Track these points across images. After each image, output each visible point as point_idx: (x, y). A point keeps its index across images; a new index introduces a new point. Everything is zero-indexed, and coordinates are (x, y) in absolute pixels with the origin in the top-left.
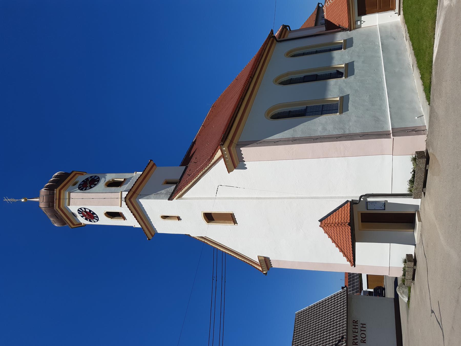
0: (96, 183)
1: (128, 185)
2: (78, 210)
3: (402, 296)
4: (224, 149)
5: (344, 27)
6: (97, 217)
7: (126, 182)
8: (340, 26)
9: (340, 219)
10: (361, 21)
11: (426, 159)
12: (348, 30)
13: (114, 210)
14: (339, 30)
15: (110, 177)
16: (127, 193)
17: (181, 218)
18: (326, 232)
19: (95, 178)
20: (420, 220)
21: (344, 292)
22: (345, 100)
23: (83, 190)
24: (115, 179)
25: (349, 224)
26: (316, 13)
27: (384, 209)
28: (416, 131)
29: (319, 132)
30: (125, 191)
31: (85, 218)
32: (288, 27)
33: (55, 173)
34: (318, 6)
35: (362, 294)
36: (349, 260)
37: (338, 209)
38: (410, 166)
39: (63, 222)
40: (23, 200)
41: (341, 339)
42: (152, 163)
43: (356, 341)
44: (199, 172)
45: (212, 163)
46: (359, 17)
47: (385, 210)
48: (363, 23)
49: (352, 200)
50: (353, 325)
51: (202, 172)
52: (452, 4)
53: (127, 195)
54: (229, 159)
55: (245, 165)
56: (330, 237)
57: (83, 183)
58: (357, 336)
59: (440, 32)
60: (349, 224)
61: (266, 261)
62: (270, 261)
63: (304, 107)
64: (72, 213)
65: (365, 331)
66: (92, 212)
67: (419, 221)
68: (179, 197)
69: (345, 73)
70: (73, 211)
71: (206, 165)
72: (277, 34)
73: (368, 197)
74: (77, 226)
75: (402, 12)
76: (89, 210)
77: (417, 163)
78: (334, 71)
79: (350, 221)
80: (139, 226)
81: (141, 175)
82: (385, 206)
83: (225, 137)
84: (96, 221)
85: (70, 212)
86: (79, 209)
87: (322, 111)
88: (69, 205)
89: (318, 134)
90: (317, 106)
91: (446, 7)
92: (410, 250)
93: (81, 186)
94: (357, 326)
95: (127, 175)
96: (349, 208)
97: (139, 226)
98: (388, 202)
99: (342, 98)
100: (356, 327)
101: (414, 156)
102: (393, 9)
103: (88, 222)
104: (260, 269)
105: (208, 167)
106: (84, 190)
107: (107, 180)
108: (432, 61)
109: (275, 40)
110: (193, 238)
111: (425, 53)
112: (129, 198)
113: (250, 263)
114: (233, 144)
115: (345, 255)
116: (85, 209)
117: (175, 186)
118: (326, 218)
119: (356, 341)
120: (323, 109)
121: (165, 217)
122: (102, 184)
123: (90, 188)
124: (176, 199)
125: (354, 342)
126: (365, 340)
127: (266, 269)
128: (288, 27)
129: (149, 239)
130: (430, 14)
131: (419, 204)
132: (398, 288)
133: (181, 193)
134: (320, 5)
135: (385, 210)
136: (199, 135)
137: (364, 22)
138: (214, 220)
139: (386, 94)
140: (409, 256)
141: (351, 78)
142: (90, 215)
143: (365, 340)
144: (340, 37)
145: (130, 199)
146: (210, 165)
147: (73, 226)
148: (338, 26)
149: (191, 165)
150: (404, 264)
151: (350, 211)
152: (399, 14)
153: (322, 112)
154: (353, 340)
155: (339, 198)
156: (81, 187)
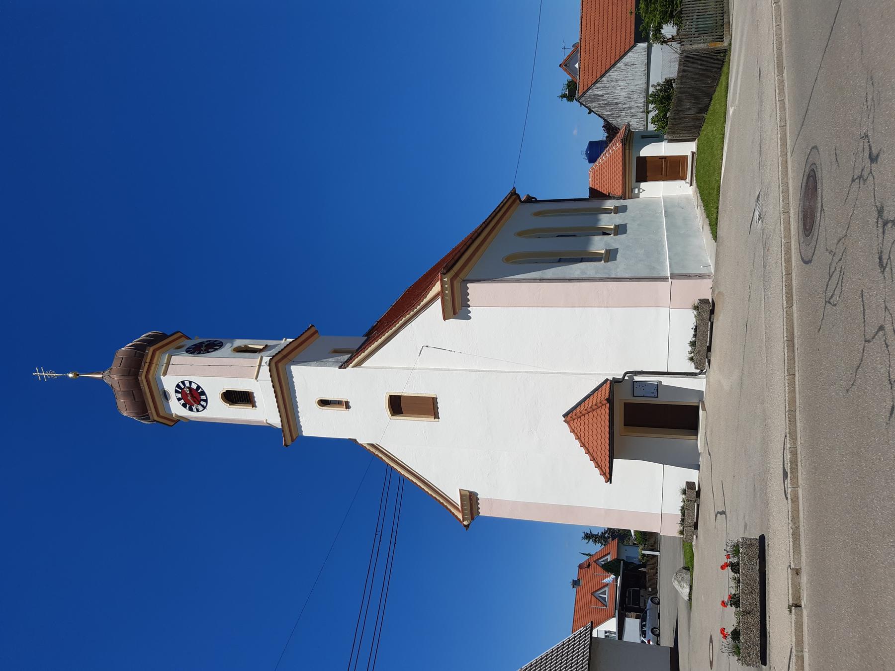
4: (446, 280)
6: (206, 401)
8: (610, 195)
10: (639, 189)
15: (239, 343)
19: (216, 343)
24: (250, 346)
27: (656, 396)
29: (577, 274)
31: (183, 402)
36: (603, 473)
39: (142, 410)
40: (71, 375)
46: (638, 183)
48: (641, 192)
49: (613, 378)
51: (404, 319)
54: (449, 304)
55: (470, 312)
61: (471, 500)
62: (477, 502)
64: (165, 391)
70: (166, 388)
74: (161, 421)
75: (694, 182)
84: (200, 408)
88: (165, 374)
89: (576, 276)
92: (693, 476)
98: (663, 384)
102: (683, 178)
103: (184, 412)
104: (460, 516)
109: (518, 200)
110: (361, 447)
112: (275, 361)
113: (445, 504)
115: (598, 466)
116: (190, 383)
118: (573, 411)
121: (324, 403)
122: (227, 348)
124: (353, 367)
127: (469, 517)
129: (286, 445)
131: (704, 389)
135: (657, 397)
137: (644, 190)
138: (403, 413)
139: (666, 250)
140: (690, 485)
144: (610, 204)
145: (277, 364)
147: (156, 418)
148: (608, 194)
152: (691, 185)
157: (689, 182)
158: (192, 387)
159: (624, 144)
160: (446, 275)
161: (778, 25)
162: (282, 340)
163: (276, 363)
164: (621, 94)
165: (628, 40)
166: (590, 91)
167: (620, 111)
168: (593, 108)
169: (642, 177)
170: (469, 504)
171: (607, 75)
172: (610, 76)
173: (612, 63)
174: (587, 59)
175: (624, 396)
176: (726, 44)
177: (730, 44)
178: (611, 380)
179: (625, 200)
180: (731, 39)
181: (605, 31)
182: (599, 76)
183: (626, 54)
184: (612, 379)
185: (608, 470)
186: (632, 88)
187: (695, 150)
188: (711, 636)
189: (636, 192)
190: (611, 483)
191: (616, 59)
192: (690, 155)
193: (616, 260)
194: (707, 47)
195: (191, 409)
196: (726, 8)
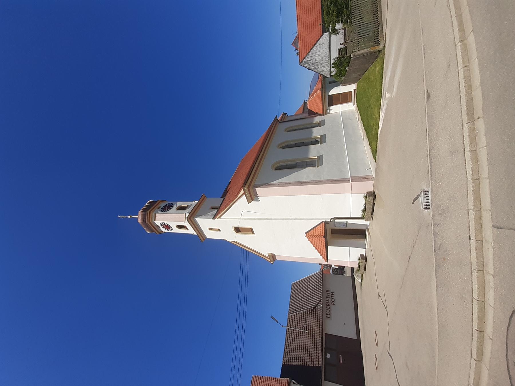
0: (171, 207)
1: (189, 209)
2: (161, 224)
3: (357, 278)
4: (245, 189)
5: (351, 9)
6: (172, 228)
7: (188, 207)
9: (318, 233)
10: (330, 110)
11: (373, 197)
12: (322, 115)
14: (317, 115)
15: (179, 204)
16: (188, 214)
17: (220, 230)
18: (309, 240)
20: (369, 234)
21: (321, 272)
22: (320, 158)
24: (183, 206)
25: (324, 237)
26: (303, 106)
28: (366, 178)
30: (187, 213)
32: (286, 114)
33: (148, 201)
34: (305, 102)
35: (331, 271)
37: (317, 226)
38: (363, 201)
40: (129, 217)
41: (319, 302)
42: (204, 196)
43: (328, 303)
44: (230, 202)
45: (238, 197)
46: (329, 107)
47: (346, 227)
50: (327, 293)
52: (392, 96)
53: (188, 216)
54: (248, 195)
55: (259, 199)
56: (312, 243)
58: (329, 300)
59: (384, 114)
60: (324, 237)
61: (273, 256)
63: (295, 162)
65: (334, 297)
67: (369, 235)
68: (219, 218)
69: (321, 141)
70: (157, 224)
71: (234, 199)
72: (279, 118)
73: (336, 219)
75: (356, 103)
77: (368, 199)
78: (314, 140)
80: (196, 234)
81: (197, 203)
82: (346, 225)
83: (246, 182)
84: (171, 230)
88: (155, 221)
89: (304, 180)
91: (388, 99)
94: (329, 293)
95: (189, 203)
96: (324, 226)
97: (196, 234)
99: (318, 157)
100: (329, 294)
101: (365, 194)
102: (350, 101)
103: (166, 231)
105: (236, 200)
107: (177, 206)
108: (378, 134)
111: (372, 129)
114: (251, 186)
115: (321, 255)
116: (164, 223)
117: (216, 210)
119: (328, 303)
121: (211, 229)
122: (175, 208)
124: (217, 219)
125: (327, 304)
126: (334, 303)
127: (273, 261)
128: (286, 114)
129: (202, 242)
130: (376, 104)
131: (369, 224)
132: (354, 273)
133: (220, 215)
134: (306, 101)
136: (233, 178)
137: (332, 110)
138: (240, 231)
141: (324, 145)
142: (168, 227)
143: (334, 303)
144: (317, 120)
145: (190, 218)
146: (237, 199)
147: (158, 233)
149: (227, 197)
150: (359, 261)
151: (325, 228)
153: (306, 166)
154: (327, 302)
155: (317, 219)
156: (162, 210)
157: (353, 103)
159: (322, 91)
160: (245, 187)
161: (466, 66)
162: (193, 201)
163: (189, 218)
164: (318, 58)
165: (319, 32)
166: (305, 59)
167: (318, 65)
168: (307, 66)
169: (331, 104)
170: (272, 259)
171: (311, 51)
172: (313, 51)
173: (313, 45)
174: (302, 44)
175: (332, 226)
176: (381, 47)
177: (384, 47)
178: (325, 222)
179: (324, 116)
180: (385, 43)
181: (309, 29)
182: (308, 52)
183: (319, 40)
185: (326, 257)
186: (323, 54)
187: (355, 87)
189: (329, 111)
191: (315, 43)
192: (353, 90)
193: (323, 165)
194: (369, 51)
196: (380, 21)
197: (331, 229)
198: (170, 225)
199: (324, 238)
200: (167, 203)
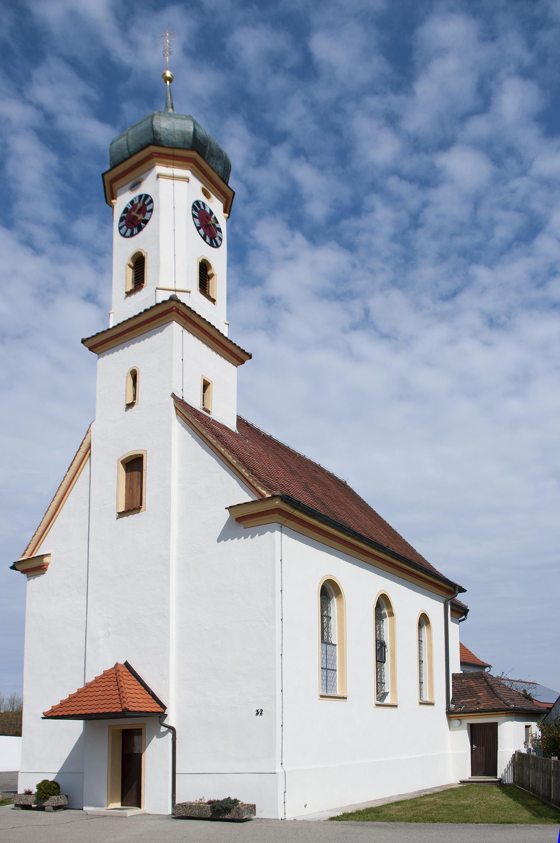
0: (208, 240)
2: (147, 196)
6: (132, 235)
13: (148, 273)
23: (192, 210)
32: (463, 617)
57: (208, 211)
66: (143, 224)
76: (200, 231)
79: (131, 711)
84: (123, 231)
85: (142, 176)
86: (149, 199)
87: (327, 669)
90: (335, 661)
93: (202, 207)
106: (194, 212)
120: (328, 671)
121: (134, 375)
123: (197, 225)
158: (147, 213)
178: (163, 713)
184: (165, 713)
188: (12, 809)
190: (43, 718)
195: (122, 219)
197: (141, 729)
198: (141, 233)
199: (123, 711)
200: (222, 223)
